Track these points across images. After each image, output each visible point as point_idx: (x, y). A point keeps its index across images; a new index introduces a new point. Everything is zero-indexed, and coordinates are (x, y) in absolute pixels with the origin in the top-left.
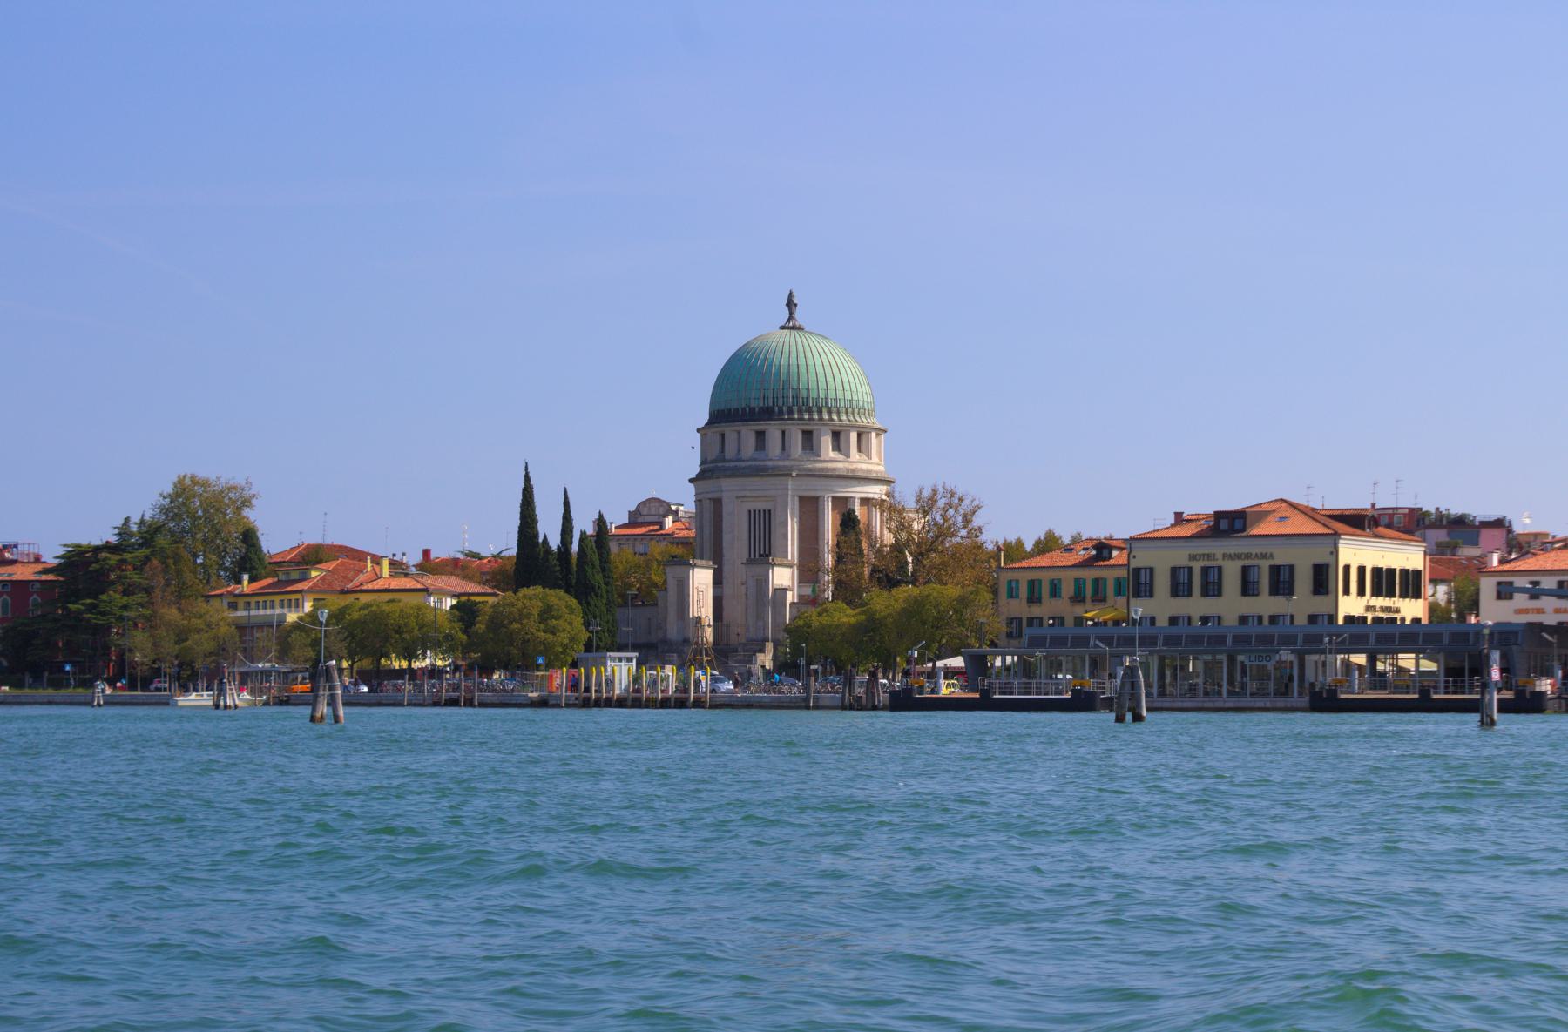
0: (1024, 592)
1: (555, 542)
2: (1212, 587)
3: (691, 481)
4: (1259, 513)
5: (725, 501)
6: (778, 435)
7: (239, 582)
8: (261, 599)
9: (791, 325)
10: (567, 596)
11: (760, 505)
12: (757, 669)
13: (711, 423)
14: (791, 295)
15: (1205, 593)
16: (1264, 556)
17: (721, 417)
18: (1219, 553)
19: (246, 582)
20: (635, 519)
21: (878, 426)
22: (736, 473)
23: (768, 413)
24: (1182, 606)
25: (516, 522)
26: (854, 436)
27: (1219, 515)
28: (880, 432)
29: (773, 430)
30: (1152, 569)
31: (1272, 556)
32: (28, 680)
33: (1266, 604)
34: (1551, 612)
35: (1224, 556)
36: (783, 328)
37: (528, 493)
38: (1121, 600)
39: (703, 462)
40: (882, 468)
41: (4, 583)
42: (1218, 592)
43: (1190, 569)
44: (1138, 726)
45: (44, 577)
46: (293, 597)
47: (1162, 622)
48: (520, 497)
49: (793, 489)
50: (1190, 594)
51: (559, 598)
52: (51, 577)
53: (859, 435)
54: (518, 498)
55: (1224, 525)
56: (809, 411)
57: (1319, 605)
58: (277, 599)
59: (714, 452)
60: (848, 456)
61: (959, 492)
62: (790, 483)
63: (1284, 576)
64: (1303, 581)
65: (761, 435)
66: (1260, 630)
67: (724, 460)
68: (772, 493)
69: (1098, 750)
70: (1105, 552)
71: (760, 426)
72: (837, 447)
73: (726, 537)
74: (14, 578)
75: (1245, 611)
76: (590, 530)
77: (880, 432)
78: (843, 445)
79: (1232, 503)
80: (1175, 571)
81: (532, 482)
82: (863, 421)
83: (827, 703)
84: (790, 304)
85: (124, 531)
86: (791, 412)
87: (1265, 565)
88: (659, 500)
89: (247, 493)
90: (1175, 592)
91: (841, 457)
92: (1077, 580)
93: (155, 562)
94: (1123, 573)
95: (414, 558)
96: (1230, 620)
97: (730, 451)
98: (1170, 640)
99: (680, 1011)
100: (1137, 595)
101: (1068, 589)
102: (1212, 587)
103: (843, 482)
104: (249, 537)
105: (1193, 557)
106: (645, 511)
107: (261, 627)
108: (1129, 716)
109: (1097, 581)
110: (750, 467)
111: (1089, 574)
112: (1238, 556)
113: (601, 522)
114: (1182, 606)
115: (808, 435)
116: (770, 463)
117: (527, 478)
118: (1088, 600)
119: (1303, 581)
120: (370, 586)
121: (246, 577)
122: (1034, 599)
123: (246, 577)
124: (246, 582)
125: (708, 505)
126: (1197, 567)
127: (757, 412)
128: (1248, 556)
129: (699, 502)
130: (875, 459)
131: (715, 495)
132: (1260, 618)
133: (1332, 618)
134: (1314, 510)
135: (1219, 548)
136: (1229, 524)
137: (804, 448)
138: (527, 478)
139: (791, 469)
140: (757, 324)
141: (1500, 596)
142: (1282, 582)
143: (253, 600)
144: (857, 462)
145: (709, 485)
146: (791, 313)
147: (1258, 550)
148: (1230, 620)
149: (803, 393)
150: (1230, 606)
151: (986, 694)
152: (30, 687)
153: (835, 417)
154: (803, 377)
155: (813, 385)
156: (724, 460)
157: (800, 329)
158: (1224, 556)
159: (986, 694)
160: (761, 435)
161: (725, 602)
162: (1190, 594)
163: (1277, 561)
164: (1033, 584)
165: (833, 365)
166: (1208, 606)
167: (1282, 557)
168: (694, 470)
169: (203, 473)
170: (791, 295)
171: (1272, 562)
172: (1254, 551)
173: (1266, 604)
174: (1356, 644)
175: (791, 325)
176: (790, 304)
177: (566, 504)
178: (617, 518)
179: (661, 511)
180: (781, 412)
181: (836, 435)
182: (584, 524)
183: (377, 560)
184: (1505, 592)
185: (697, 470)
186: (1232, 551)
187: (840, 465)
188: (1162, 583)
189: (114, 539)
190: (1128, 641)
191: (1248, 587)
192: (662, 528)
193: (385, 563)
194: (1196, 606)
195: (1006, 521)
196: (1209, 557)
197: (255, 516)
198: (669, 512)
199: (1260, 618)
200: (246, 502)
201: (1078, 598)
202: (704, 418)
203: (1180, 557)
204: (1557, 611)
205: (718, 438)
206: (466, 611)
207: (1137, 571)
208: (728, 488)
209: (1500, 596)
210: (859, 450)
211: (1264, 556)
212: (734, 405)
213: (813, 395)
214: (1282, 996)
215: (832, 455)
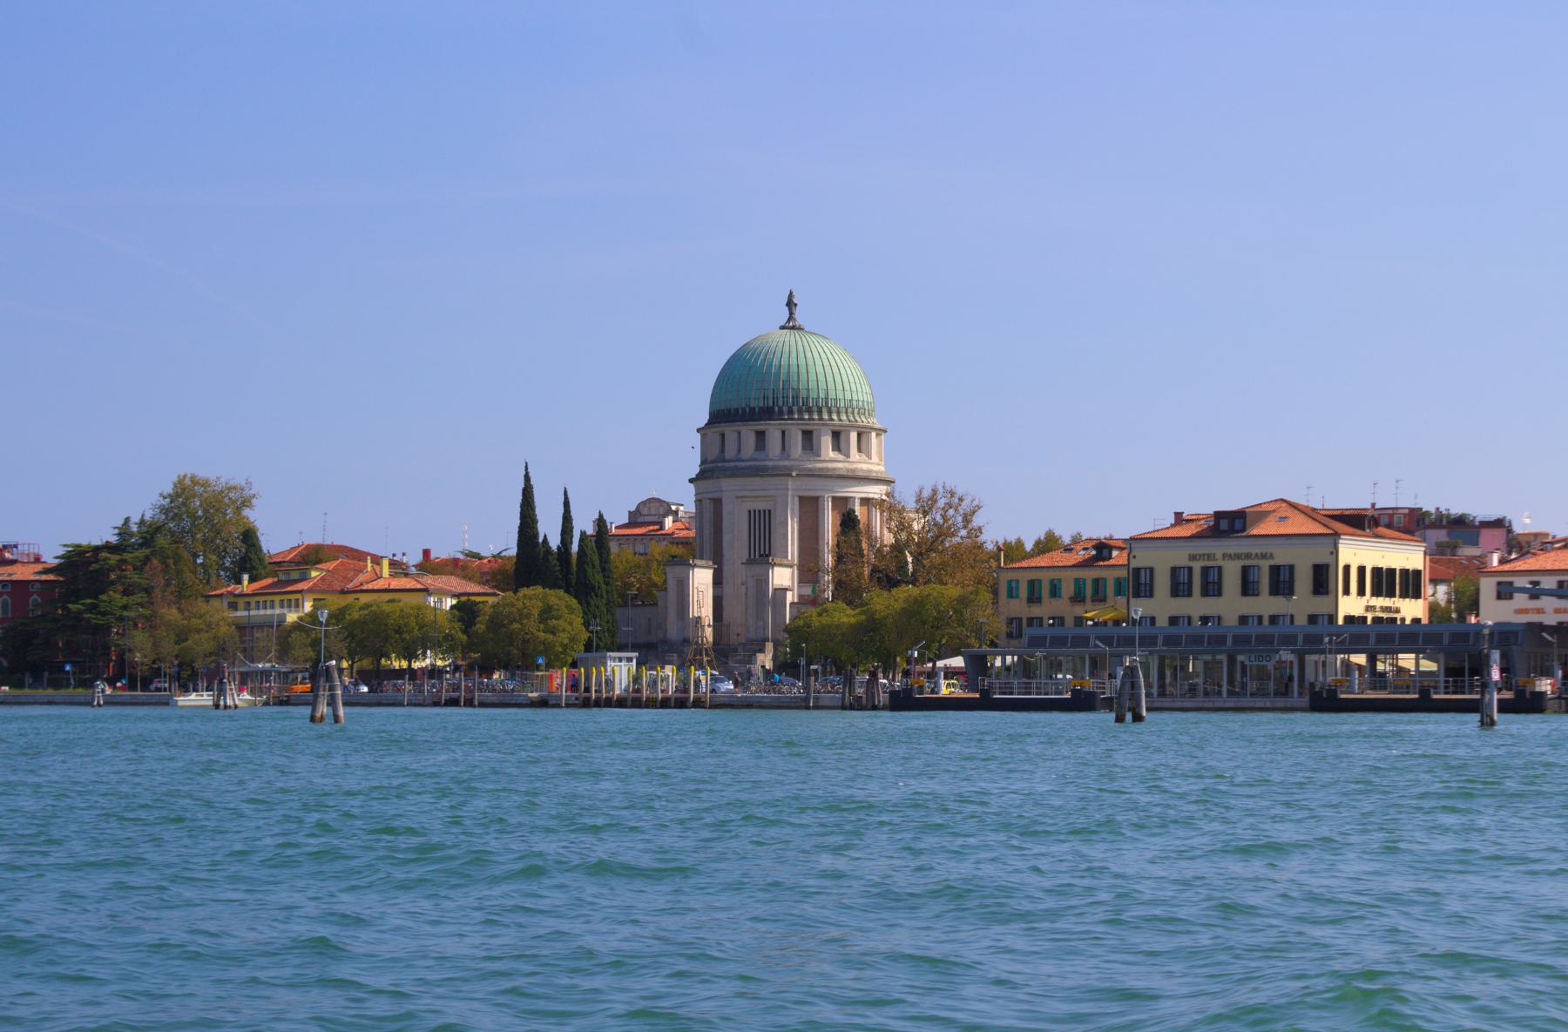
0: (1024, 592)
1: (555, 542)
2: (1212, 587)
3: (691, 481)
4: (1259, 513)
5: (725, 501)
6: (778, 434)
7: (239, 582)
8: (261, 599)
9: (791, 325)
10: (567, 596)
11: (760, 506)
12: (757, 669)
13: (710, 423)
14: (791, 295)
15: (1205, 593)
16: (1264, 556)
17: (721, 417)
18: (1219, 553)
19: (246, 583)
20: (635, 519)
21: (878, 426)
22: (736, 473)
23: (768, 413)
24: (1182, 606)
25: (516, 522)
26: (854, 436)
27: (1219, 515)
28: (880, 432)
29: (773, 430)
30: (1152, 570)
31: (1272, 556)
32: (28, 680)
33: (1266, 604)
34: (1551, 612)
35: (1224, 556)
36: (783, 328)
37: (528, 493)
38: (1121, 600)
39: (703, 462)
40: (882, 468)
41: (4, 583)
42: (1218, 593)
43: (1190, 569)
44: (1139, 727)
45: (44, 577)
46: (293, 597)
47: (1162, 622)
48: (520, 497)
49: (793, 489)
50: (1190, 594)
51: (559, 598)
52: (51, 577)
53: (859, 435)
54: (518, 498)
55: (1224, 525)
56: (809, 411)
57: (1319, 605)
58: (277, 599)
59: (714, 452)
60: (848, 456)
61: (960, 492)
62: (790, 483)
63: (1284, 576)
64: (1303, 581)
65: (761, 435)
66: (1260, 630)
67: (724, 460)
68: (772, 493)
69: (1098, 750)
70: (1105, 552)
71: (761, 426)
72: (837, 447)
73: (726, 537)
74: (15, 578)
75: (1245, 612)
76: (590, 530)
77: (880, 432)
78: (843, 445)
79: (1232, 503)
80: (1175, 571)
81: (532, 482)
82: (863, 421)
83: (827, 703)
84: (790, 304)
85: (124, 531)
86: (791, 412)
87: (1265, 565)
88: (659, 500)
89: (247, 493)
90: (1175, 592)
91: (841, 457)
92: (1077, 580)
93: (155, 562)
94: (1123, 573)
95: (413, 558)
96: (1231, 620)
97: (730, 451)
98: (1170, 640)
99: (680, 1011)
100: (1137, 595)
101: (1068, 590)
102: (1212, 587)
103: (844, 483)
104: (249, 537)
105: (1193, 558)
106: (645, 511)
107: (261, 626)
108: (1129, 716)
109: (1097, 581)
110: (750, 467)
111: (1089, 574)
112: (1238, 556)
113: (601, 522)
114: (1182, 606)
115: (808, 435)
116: (770, 464)
117: (527, 478)
118: (1088, 599)
119: (1303, 581)
120: (370, 586)
121: (246, 577)
122: (1034, 599)
123: (246, 577)
124: (246, 583)
125: (708, 506)
126: (1197, 567)
127: (757, 412)
128: (1248, 556)
129: (699, 502)
130: (875, 459)
131: (715, 495)
132: (1260, 618)
133: (1332, 618)
134: (1314, 510)
135: (1218, 548)
136: (1229, 524)
137: (804, 448)
138: (527, 478)
139: (791, 469)
140: (757, 324)
141: (1500, 596)
142: (1282, 582)
143: (253, 600)
144: (857, 462)
145: (708, 485)
146: (791, 313)
147: (1258, 551)
148: (1231, 620)
149: (803, 393)
150: (1230, 606)
151: (986, 694)
152: (30, 687)
153: (835, 417)
154: (803, 377)
155: (813, 385)
156: (724, 460)
157: (800, 329)
158: (1224, 556)
159: (986, 694)
160: (761, 435)
161: (725, 602)
162: (1190, 594)
163: (1277, 561)
164: (1033, 584)
165: (833, 365)
166: (1209, 606)
167: (1282, 557)
168: (694, 470)
169: (203, 473)
170: (791, 295)
171: (1272, 562)
172: (1254, 551)
173: (1266, 604)
174: (1355, 644)
175: (791, 325)
176: (790, 304)
177: (566, 504)
178: (617, 518)
179: (661, 511)
180: (781, 412)
181: (836, 435)
182: (584, 524)
183: (377, 560)
184: (1505, 592)
185: (697, 470)
186: (1232, 551)
187: (840, 465)
188: (1162, 583)
189: (114, 539)
190: (1128, 641)
191: (1248, 587)
192: (662, 528)
193: (385, 563)
194: (1196, 606)
195: (1006, 521)
196: (1210, 557)
197: (255, 516)
198: (669, 512)
199: (1260, 618)
200: (246, 502)
201: (1078, 598)
202: (704, 418)
203: (1180, 557)
204: (1557, 611)
205: (717, 439)
206: (466, 611)
207: (1137, 571)
208: (728, 488)
209: (1500, 596)
210: (859, 450)
211: (1264, 556)
212: (734, 405)
213: (813, 395)
214: (1282, 996)
215: (832, 454)
